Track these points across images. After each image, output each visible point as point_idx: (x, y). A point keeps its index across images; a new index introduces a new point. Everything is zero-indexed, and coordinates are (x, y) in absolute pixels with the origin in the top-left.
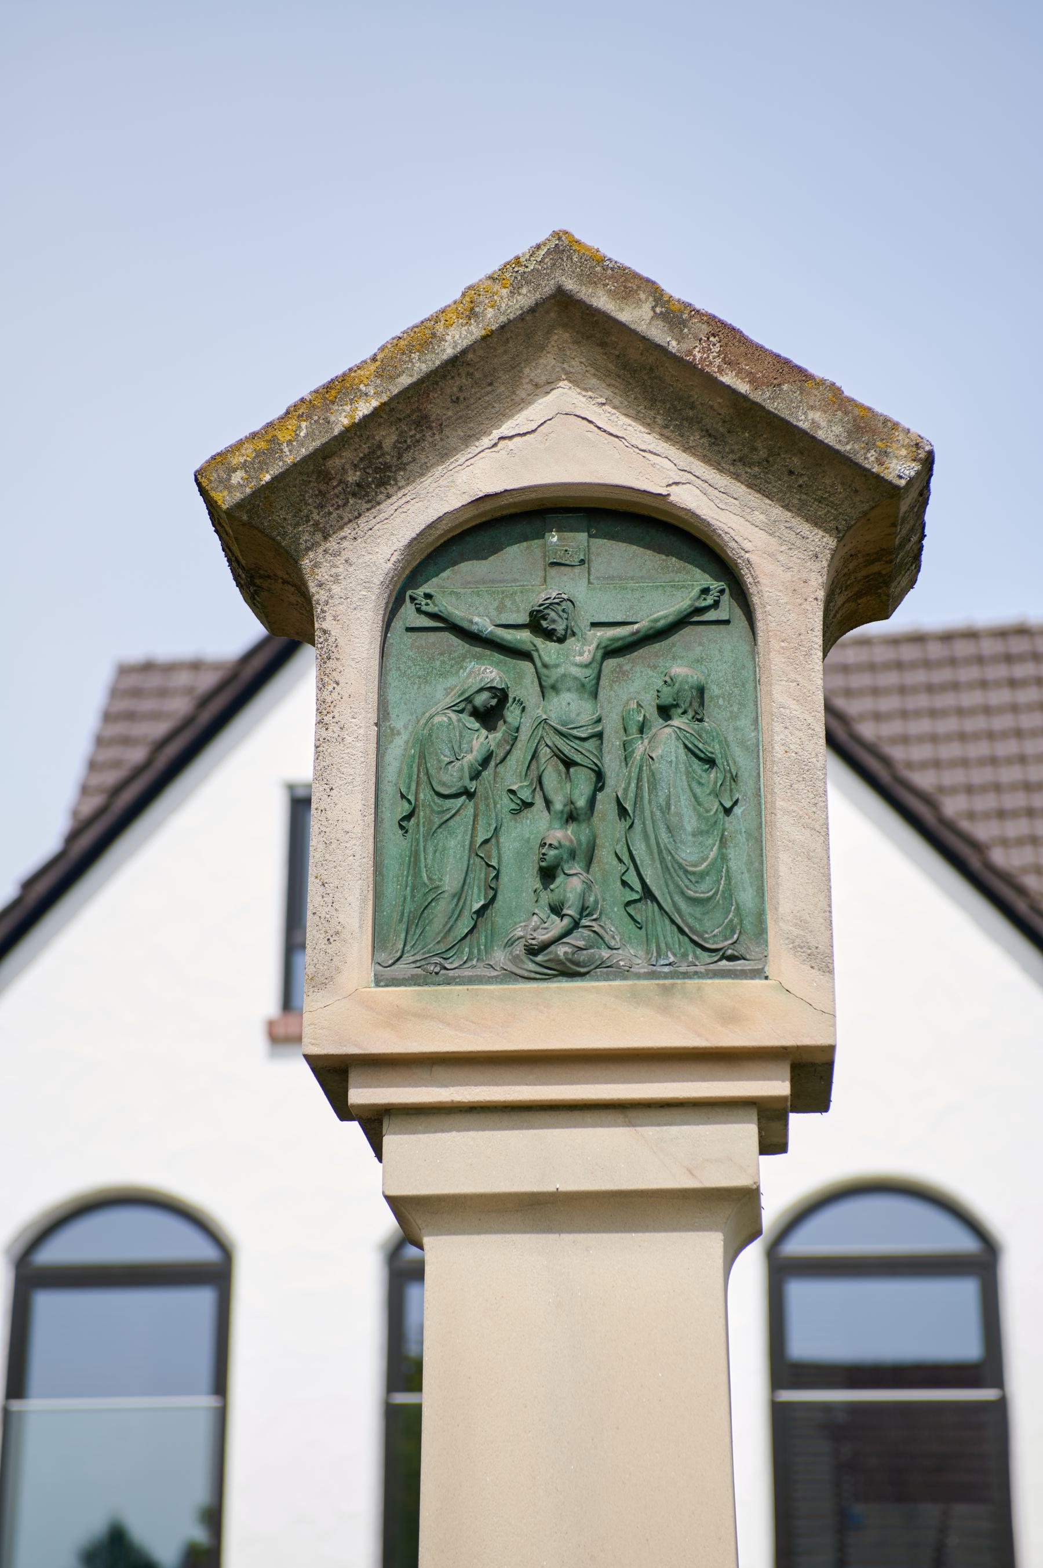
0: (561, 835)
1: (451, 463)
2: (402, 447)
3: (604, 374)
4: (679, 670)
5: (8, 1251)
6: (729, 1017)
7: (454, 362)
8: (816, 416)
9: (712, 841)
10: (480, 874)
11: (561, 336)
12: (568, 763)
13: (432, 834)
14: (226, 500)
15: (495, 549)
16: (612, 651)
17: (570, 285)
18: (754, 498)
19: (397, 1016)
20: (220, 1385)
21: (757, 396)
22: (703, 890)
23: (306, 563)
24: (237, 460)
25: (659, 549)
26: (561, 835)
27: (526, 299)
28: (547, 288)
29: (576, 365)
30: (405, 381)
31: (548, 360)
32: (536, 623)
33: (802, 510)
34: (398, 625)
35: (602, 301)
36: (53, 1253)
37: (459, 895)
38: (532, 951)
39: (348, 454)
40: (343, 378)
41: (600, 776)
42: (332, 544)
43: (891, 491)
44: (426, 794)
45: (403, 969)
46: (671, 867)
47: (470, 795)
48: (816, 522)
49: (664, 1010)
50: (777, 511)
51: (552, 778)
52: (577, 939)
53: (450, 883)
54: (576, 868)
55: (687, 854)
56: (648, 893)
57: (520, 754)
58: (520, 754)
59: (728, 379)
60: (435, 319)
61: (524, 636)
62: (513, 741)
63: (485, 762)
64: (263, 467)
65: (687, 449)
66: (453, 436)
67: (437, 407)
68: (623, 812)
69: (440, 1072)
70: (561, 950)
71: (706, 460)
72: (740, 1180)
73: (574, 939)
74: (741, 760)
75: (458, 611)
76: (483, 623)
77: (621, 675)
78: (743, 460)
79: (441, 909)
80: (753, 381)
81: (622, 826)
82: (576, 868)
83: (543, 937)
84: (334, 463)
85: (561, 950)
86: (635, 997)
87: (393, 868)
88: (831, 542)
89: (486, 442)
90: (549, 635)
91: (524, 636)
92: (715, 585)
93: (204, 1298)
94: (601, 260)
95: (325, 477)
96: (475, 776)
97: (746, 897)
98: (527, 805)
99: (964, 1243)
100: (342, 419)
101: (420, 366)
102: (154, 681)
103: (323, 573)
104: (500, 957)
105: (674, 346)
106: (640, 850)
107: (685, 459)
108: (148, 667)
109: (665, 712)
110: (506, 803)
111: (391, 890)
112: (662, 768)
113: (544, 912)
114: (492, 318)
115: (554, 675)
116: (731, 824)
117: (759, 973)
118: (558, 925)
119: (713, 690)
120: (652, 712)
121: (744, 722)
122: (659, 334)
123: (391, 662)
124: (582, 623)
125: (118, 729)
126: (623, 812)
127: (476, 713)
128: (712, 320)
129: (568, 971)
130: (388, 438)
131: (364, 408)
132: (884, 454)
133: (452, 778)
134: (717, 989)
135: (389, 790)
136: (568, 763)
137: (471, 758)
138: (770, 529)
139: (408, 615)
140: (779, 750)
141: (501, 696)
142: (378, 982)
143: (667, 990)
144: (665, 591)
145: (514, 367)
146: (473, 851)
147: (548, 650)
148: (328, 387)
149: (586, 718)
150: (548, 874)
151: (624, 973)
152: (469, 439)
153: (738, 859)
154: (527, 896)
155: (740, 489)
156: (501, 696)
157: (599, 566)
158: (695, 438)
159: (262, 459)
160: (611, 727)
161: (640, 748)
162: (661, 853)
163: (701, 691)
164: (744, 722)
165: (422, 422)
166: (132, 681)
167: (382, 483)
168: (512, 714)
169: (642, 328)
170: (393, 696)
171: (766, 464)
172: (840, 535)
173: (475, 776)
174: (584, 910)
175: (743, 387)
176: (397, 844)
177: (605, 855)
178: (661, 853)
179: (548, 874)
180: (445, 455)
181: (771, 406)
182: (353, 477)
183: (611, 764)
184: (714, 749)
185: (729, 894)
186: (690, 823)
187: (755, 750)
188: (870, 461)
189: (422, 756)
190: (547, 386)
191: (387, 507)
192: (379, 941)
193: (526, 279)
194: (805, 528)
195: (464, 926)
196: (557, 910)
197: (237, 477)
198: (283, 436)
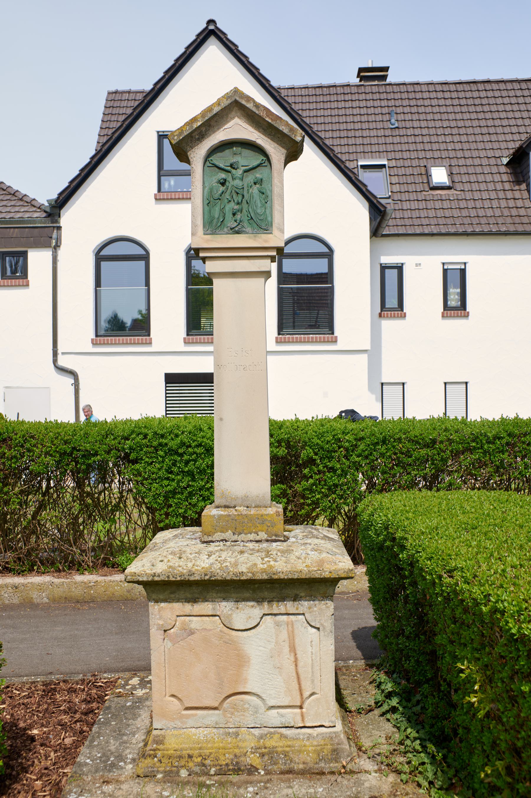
0: (236, 207)
1: (215, 134)
2: (206, 131)
3: (244, 116)
4: (258, 176)
5: (93, 252)
6: (266, 241)
7: (216, 114)
8: (283, 127)
9: (263, 208)
10: (222, 214)
11: (236, 108)
12: (238, 193)
13: (213, 207)
14: (174, 142)
15: (224, 151)
16: (246, 171)
17: (238, 99)
18: (272, 142)
19: (207, 241)
20: (147, 284)
21: (273, 123)
22: (261, 218)
23: (189, 154)
24: (175, 134)
25: (254, 151)
26: (236, 207)
27: (229, 102)
28: (233, 99)
29: (239, 114)
30: (207, 118)
31: (233, 113)
32: (231, 166)
33: (280, 145)
34: (206, 165)
35: (244, 102)
36: (105, 252)
37: (218, 218)
38: (231, 229)
39: (196, 133)
40: (195, 117)
41: (243, 196)
42: (193, 150)
43: (297, 143)
44: (212, 199)
45: (209, 232)
46: (256, 214)
47: (220, 199)
48: (283, 147)
49: (255, 240)
50: (276, 145)
51: (234, 197)
52: (239, 227)
53: (216, 216)
54: (239, 213)
55: (259, 211)
56: (252, 218)
57: (229, 191)
58: (229, 191)
59: (267, 119)
60: (212, 105)
61: (229, 168)
62: (227, 189)
63: (222, 193)
64: (180, 135)
65: (259, 132)
66: (216, 128)
67: (213, 123)
68: (247, 203)
69: (215, 251)
70: (237, 229)
71: (263, 134)
72: (267, 269)
73: (238, 227)
74: (269, 193)
75: (217, 163)
76: (222, 166)
77: (247, 176)
78: (270, 135)
79: (215, 221)
80: (272, 120)
81: (247, 205)
82: (239, 213)
83: (233, 226)
84: (194, 134)
85: (237, 229)
86: (250, 238)
87: (206, 213)
88: (286, 151)
89: (222, 129)
90: (234, 168)
91: (229, 168)
92: (265, 159)
93: (143, 263)
94: (243, 93)
95: (192, 137)
96: (221, 196)
97: (269, 219)
98: (230, 201)
99: (325, 250)
100: (195, 126)
101: (209, 115)
102: (118, 97)
103: (192, 156)
104: (226, 230)
105: (257, 112)
106: (250, 210)
107: (259, 134)
108: (116, 92)
109: (255, 183)
110: (226, 201)
111: (206, 217)
112: (255, 195)
113: (233, 221)
114: (223, 105)
115: (235, 176)
116: (267, 205)
117: (271, 233)
118: (236, 224)
119: (264, 179)
120: (253, 183)
121: (269, 186)
122: (254, 109)
123: (205, 176)
124: (240, 166)
125: (110, 111)
126: (247, 203)
127: (221, 183)
128: (264, 107)
129: (238, 233)
130: (204, 129)
131: (199, 124)
132: (295, 135)
133: (217, 196)
134: (263, 236)
135: (205, 198)
136: (238, 193)
137: (220, 192)
138: (275, 148)
139: (208, 164)
140: (275, 192)
141: (225, 180)
142: (204, 234)
143: (255, 236)
144: (262, 755)
145: (227, 115)
146: (221, 210)
147: (234, 171)
148: (192, 119)
149: (241, 185)
150: (234, 214)
151: (247, 233)
152: (218, 129)
153: (268, 212)
154: (230, 218)
155: (269, 140)
156: (225, 180)
157: (243, 154)
158: (261, 130)
159: (180, 133)
160: (245, 186)
161: (250, 191)
162: (254, 211)
163: (262, 180)
164: (269, 186)
165: (210, 126)
166: (112, 97)
167: (203, 138)
168: (227, 183)
169: (251, 108)
170: (205, 180)
171: (274, 136)
172: (287, 150)
173: (221, 196)
174: (241, 221)
175: (270, 121)
176: (207, 208)
177: (244, 211)
178: (254, 211)
179: (234, 214)
180: (214, 132)
181: (275, 125)
182: (197, 137)
183: (245, 193)
184: (264, 191)
185: (266, 218)
186: (259, 205)
187: (271, 191)
188: (293, 137)
189: (211, 192)
190: (233, 118)
191: (204, 142)
192: (204, 226)
193: (229, 97)
194: (281, 148)
195: (219, 224)
196: (236, 221)
197: (176, 138)
198: (184, 129)
